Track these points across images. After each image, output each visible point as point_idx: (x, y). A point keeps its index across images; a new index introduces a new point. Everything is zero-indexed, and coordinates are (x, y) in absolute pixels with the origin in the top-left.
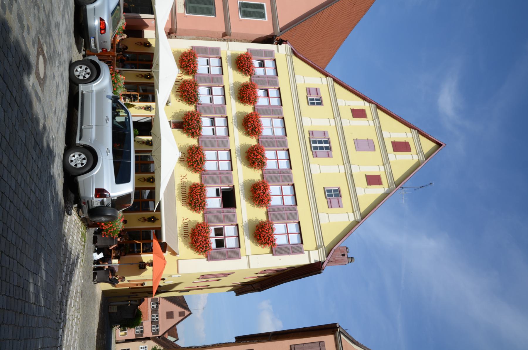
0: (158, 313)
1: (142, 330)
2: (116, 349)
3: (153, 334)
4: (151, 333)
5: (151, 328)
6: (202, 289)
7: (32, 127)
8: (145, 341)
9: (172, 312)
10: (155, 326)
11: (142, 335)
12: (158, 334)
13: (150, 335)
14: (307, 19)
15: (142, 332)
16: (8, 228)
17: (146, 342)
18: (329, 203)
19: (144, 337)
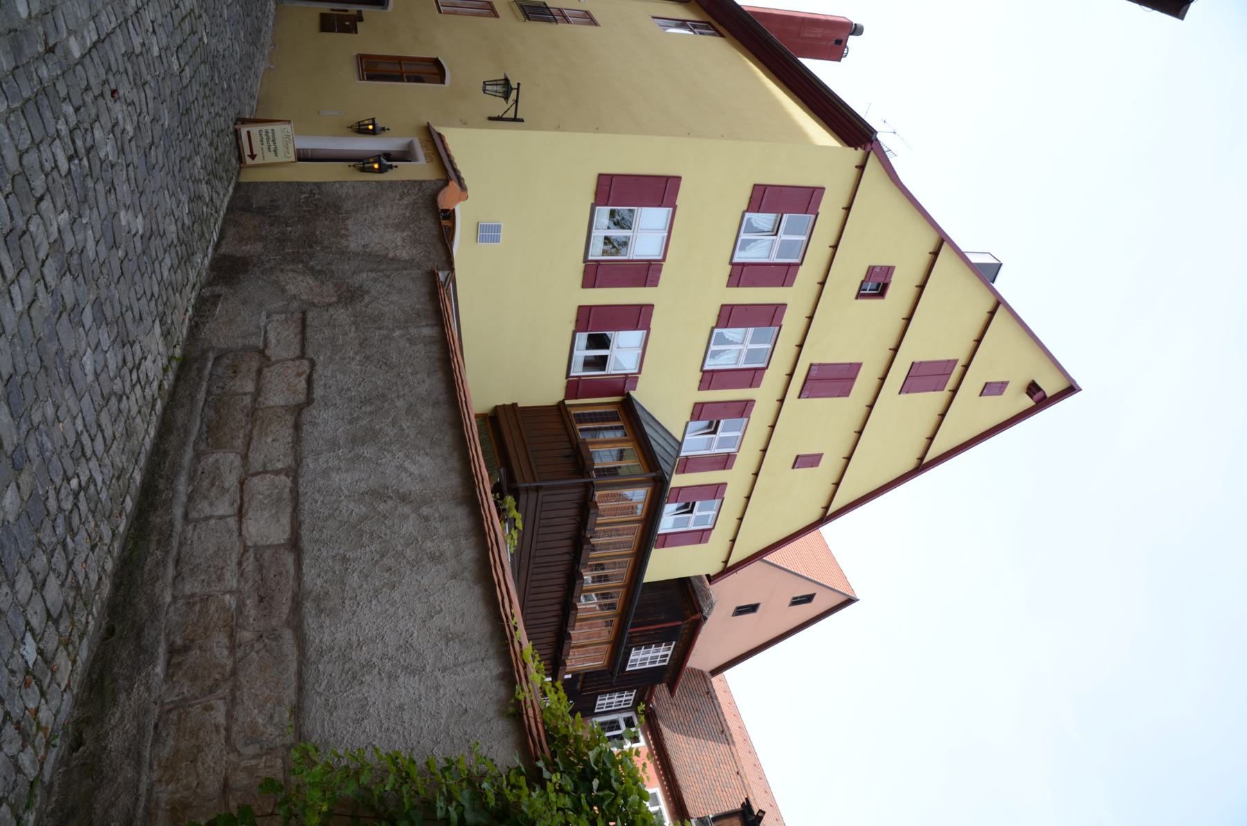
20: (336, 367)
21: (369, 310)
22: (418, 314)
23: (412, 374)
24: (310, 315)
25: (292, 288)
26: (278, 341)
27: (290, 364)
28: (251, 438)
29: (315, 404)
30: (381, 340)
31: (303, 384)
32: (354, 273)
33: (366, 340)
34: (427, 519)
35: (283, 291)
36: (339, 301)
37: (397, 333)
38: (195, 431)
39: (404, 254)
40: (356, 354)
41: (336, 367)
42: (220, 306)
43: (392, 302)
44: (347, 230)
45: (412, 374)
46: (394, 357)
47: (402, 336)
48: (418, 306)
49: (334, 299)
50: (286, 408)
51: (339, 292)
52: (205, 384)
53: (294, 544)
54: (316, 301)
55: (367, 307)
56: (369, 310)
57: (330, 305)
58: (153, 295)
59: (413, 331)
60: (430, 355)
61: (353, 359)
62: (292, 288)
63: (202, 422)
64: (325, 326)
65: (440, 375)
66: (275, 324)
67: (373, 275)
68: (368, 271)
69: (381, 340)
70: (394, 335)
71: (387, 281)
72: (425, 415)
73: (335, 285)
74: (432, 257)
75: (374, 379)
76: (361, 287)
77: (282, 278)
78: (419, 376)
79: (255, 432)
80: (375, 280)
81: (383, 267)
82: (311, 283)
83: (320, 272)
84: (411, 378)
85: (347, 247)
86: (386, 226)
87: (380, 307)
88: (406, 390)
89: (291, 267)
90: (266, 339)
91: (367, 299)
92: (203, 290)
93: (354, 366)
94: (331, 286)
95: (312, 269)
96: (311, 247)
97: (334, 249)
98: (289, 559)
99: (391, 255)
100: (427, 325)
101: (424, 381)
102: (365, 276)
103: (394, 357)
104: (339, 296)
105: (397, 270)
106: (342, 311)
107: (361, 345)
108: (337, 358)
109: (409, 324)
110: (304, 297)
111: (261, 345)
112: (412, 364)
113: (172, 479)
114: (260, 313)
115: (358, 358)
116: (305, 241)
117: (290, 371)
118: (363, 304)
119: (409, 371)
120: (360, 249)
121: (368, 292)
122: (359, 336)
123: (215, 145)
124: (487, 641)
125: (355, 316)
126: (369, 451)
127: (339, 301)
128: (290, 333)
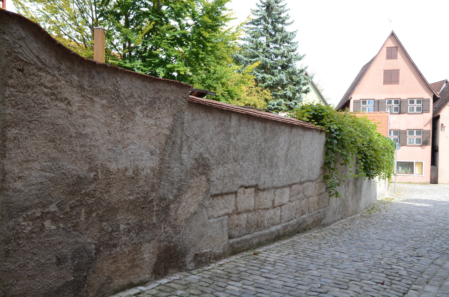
0: (406, 131)
1: (415, 132)
2: (448, 184)
3: (428, 111)
4: (425, 114)
5: (414, 115)
6: (437, 151)
7: (95, 110)
8: (440, 125)
9: (384, 74)
10: (410, 105)
11: (427, 132)
12: (428, 100)
13: (429, 116)
14: (240, 106)
15: (396, 102)
16: (289, 293)
17: (442, 125)
18: (426, 111)
19: (429, 128)
20: (245, 174)
21: (216, 155)
22: (222, 124)
23: (253, 136)
24: (214, 192)
25: (193, 208)
26: (225, 208)
27: (238, 198)
28: (265, 209)
29: (258, 183)
30: (236, 150)
31: (249, 190)
32: (182, 164)
33: (234, 158)
34: (293, 143)
35: (195, 213)
36: (206, 174)
37: (232, 139)
38: (260, 232)
39: (168, 121)
40: (239, 164)
41: (245, 174)
42: (204, 251)
43: (211, 139)
44: (126, 169)
45: (253, 136)
46: (245, 144)
47: (235, 138)
48: (217, 123)
49: (204, 178)
50: (256, 196)
51: (198, 174)
52: (243, 238)
53: (290, 186)
54: (205, 190)
55: (213, 156)
56: (216, 155)
57: (208, 180)
58: (261, 268)
59: (232, 131)
60: (246, 124)
61: (241, 166)
62: (193, 208)
63: (255, 232)
64: (223, 182)
65: (255, 122)
66: (214, 212)
67: (185, 149)
68: (181, 153)
69: (236, 150)
70: (234, 142)
71: (192, 139)
72: (269, 135)
73: (192, 177)
74: (172, 98)
75: (253, 156)
76: (196, 159)
77: (183, 217)
78: (254, 133)
79: (262, 207)
80: (190, 148)
81: (179, 141)
82: (188, 196)
83: (179, 189)
84: (255, 138)
85: (153, 170)
86: (126, 130)
87: (214, 148)
88: (259, 141)
89: (172, 214)
90: (224, 215)
91: (206, 155)
92: (191, 268)
93: (245, 165)
94: (192, 181)
95: (176, 197)
96: (152, 201)
97: (155, 181)
98: (294, 187)
99: (168, 133)
100: (230, 121)
101: (256, 132)
102: (184, 155)
103: (245, 144)
104: (201, 174)
105: (183, 130)
106: (214, 172)
107: (236, 161)
108: (240, 174)
109: (228, 132)
110: (201, 198)
111: (227, 217)
112: (249, 135)
113: (272, 233)
114: (210, 223)
115: (241, 163)
116: (143, 208)
117: (242, 198)
118: (210, 158)
119: (251, 137)
120: (156, 159)
121: (201, 155)
122: (231, 162)
123: (264, 264)
124: (280, 129)
125: (219, 163)
126: (275, 160)
127: (206, 174)
128: (220, 202)
